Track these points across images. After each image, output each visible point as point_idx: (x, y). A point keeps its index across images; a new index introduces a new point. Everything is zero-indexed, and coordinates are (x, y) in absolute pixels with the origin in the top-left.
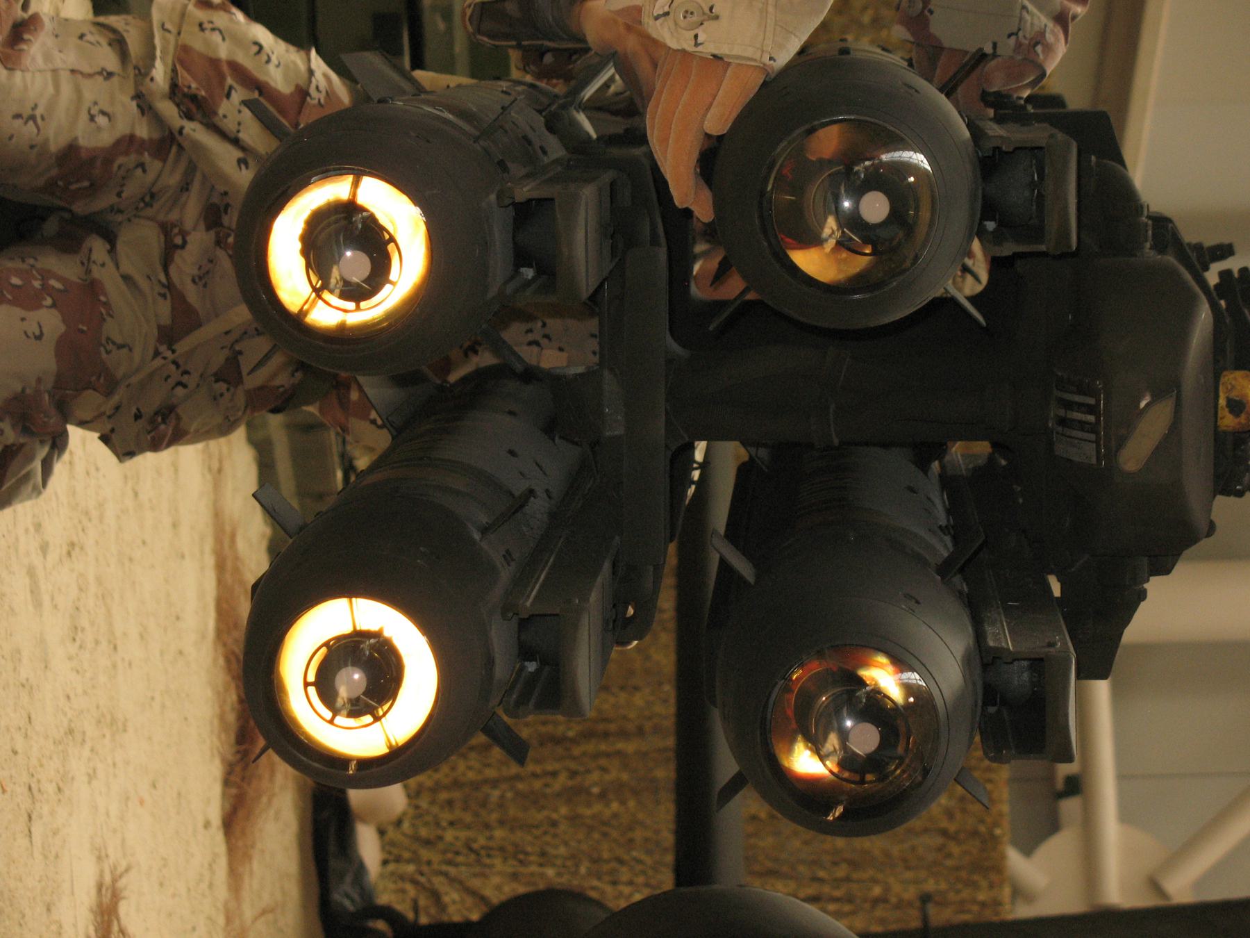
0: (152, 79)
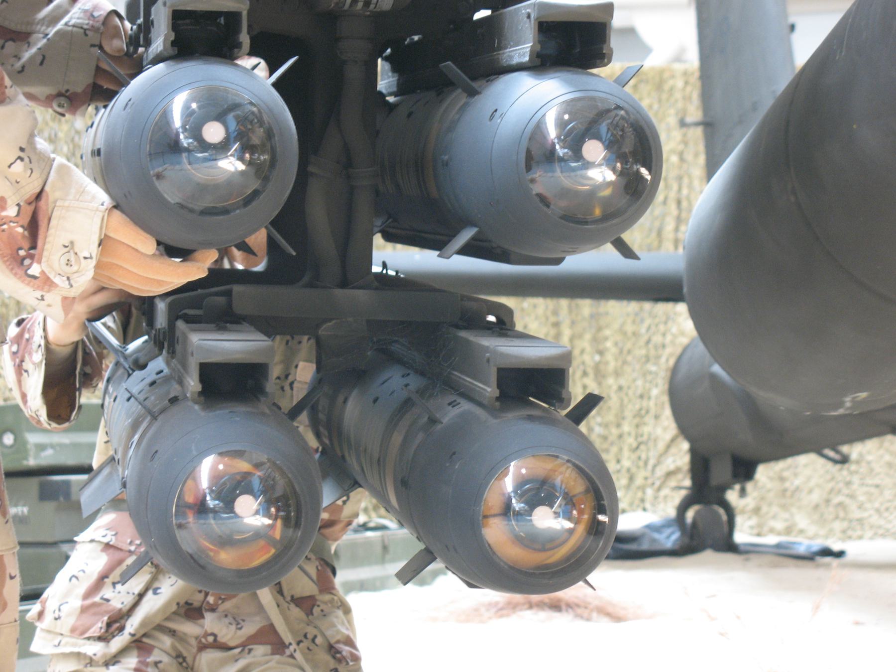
0: (95, 655)
